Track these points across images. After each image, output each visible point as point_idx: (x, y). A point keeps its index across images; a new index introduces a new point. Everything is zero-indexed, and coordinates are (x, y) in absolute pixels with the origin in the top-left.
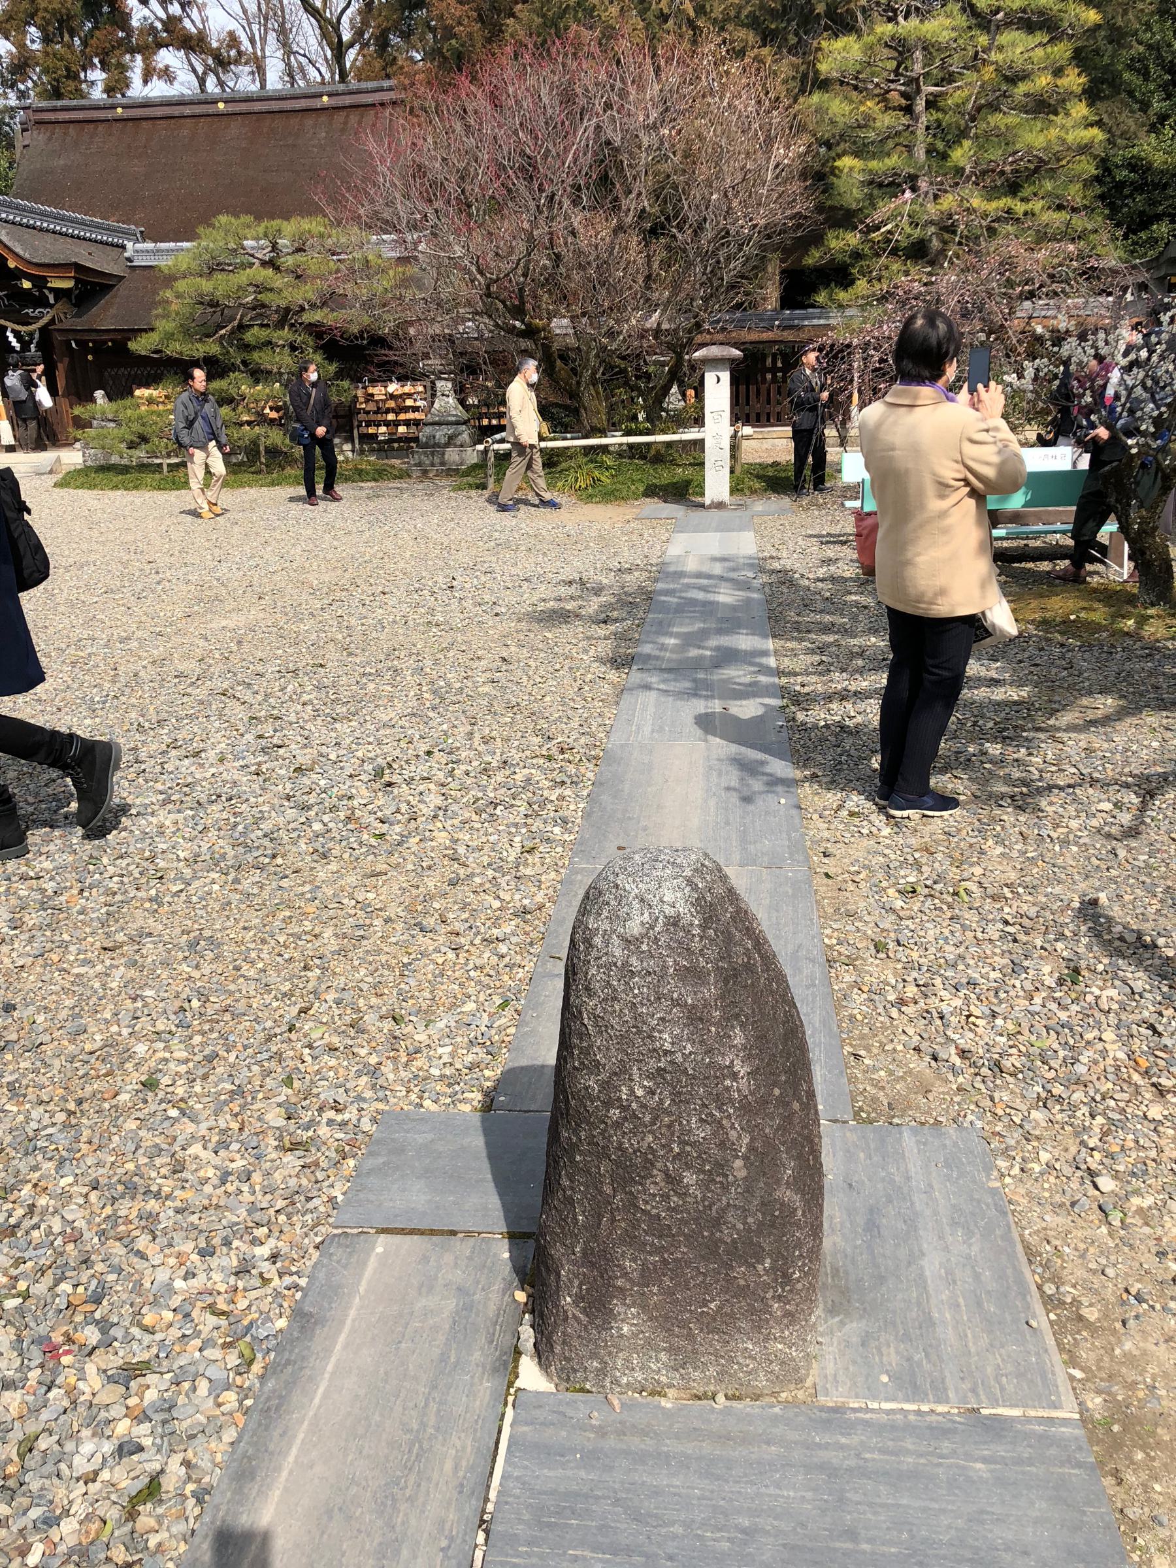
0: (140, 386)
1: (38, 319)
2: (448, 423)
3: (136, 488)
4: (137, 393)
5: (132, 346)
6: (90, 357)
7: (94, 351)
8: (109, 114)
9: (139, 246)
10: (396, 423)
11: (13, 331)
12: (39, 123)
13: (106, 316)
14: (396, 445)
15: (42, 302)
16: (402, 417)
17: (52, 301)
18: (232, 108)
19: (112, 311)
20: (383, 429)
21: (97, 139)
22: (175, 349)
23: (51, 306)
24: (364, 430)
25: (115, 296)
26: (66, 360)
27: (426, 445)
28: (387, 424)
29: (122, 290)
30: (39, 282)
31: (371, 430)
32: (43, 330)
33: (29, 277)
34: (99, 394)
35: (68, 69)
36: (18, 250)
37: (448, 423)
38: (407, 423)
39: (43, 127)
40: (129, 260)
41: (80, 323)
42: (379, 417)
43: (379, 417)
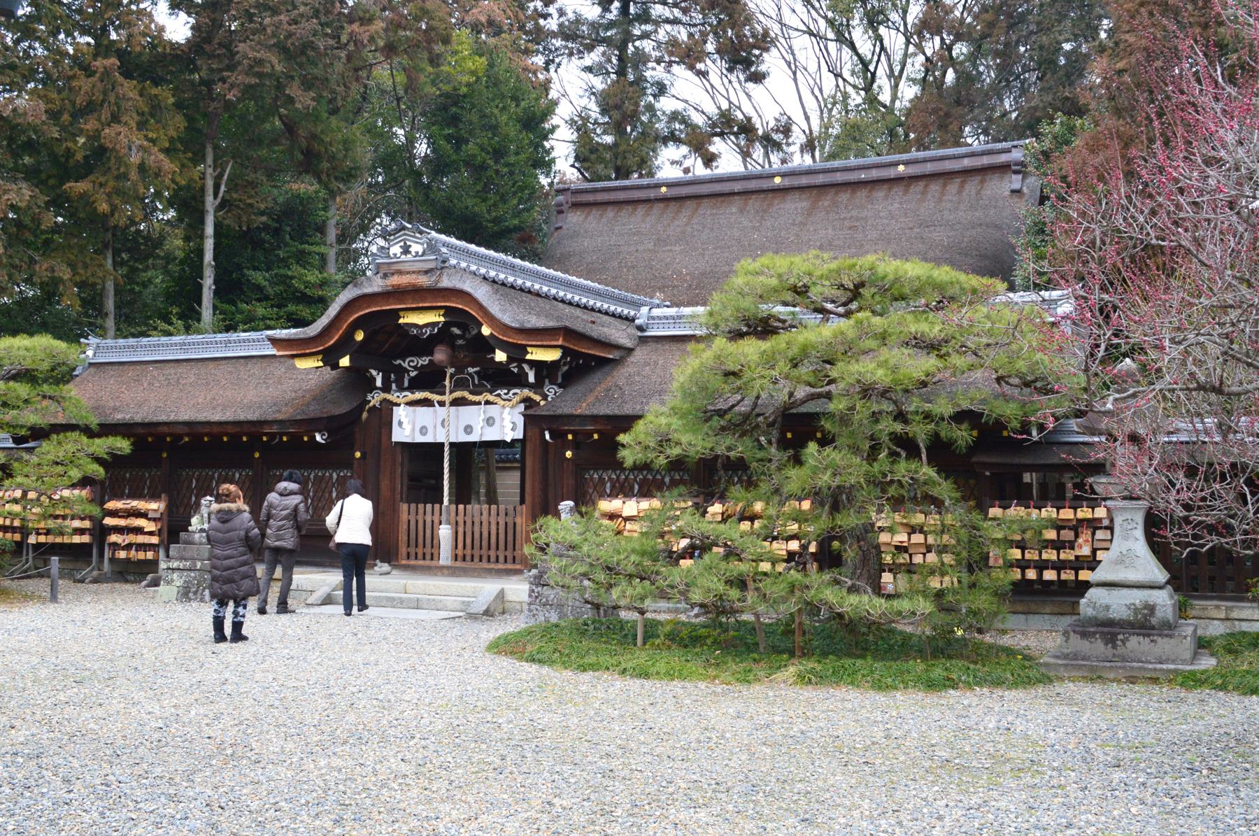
6: (569, 454)
7: (575, 446)
16: (1031, 555)
18: (788, 182)
30: (517, 353)
33: (505, 346)
40: (640, 328)
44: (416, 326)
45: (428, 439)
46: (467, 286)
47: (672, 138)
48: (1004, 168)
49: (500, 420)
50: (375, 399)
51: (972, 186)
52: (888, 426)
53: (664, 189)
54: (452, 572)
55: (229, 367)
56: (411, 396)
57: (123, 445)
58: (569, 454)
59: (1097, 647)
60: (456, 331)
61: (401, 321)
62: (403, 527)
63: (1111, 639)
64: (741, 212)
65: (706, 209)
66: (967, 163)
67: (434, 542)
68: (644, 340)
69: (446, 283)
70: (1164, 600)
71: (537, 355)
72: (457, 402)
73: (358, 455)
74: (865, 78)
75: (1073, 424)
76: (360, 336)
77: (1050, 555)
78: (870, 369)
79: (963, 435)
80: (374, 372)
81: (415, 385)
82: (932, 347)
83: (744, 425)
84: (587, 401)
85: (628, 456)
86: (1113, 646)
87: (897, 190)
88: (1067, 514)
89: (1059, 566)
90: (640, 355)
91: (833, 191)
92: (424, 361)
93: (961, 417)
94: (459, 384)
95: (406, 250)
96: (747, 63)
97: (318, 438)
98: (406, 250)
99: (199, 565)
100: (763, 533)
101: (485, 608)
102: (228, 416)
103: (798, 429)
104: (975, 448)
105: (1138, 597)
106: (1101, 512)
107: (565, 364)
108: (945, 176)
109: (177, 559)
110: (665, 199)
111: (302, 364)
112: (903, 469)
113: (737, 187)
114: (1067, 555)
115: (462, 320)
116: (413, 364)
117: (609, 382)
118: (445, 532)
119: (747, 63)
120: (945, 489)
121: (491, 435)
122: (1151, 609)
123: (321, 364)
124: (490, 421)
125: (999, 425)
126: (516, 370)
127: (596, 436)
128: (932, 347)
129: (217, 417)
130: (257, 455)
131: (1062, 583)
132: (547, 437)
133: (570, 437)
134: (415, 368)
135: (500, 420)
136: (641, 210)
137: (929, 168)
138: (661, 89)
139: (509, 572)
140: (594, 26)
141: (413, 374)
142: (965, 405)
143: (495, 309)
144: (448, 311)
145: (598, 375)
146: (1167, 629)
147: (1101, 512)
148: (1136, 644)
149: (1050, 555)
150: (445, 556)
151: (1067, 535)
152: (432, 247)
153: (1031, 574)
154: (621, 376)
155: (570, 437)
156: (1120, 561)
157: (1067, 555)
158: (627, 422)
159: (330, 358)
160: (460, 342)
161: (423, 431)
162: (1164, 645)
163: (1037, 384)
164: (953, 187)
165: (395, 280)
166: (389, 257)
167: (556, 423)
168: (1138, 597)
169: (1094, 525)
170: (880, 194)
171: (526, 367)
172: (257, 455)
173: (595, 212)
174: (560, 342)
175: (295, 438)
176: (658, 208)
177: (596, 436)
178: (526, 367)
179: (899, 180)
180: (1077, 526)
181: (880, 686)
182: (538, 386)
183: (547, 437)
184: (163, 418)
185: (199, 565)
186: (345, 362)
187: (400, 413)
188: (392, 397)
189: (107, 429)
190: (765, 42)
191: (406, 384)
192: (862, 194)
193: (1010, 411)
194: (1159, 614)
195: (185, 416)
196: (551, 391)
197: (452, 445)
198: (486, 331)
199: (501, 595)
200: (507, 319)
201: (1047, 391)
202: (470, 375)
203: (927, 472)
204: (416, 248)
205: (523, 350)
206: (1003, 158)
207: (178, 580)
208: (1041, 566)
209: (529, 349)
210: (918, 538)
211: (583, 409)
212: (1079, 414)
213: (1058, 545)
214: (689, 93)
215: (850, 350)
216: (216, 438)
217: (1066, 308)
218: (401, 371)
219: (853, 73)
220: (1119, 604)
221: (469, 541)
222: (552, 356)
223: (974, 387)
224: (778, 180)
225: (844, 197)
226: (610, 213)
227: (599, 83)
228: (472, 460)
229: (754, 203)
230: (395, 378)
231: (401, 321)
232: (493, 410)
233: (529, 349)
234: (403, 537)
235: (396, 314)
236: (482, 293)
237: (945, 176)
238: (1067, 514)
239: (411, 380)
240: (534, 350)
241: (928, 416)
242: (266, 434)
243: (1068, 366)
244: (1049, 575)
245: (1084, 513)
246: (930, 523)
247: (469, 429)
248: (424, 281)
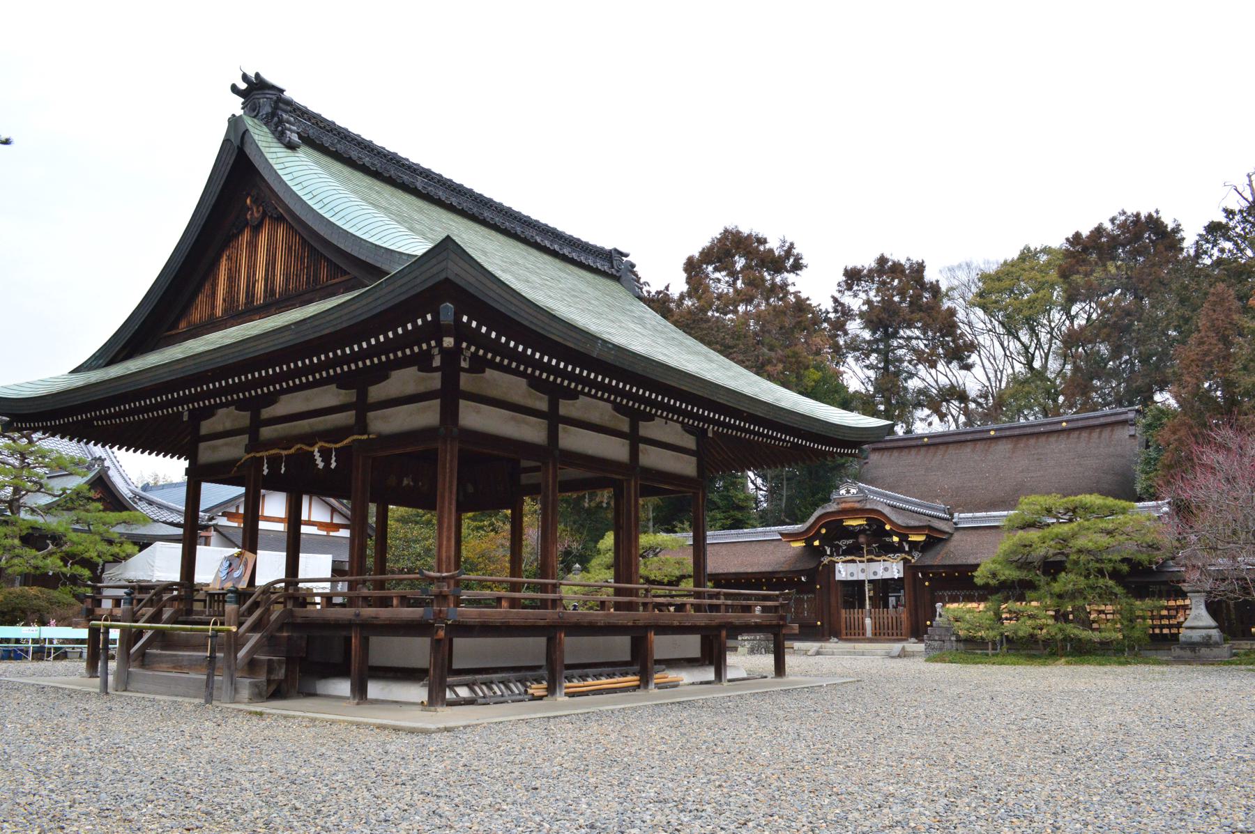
7: (930, 580)
9: (962, 515)
18: (999, 434)
30: (904, 537)
33: (897, 534)
45: (855, 578)
46: (879, 508)
47: (919, 405)
48: (1124, 423)
49: (892, 569)
50: (826, 560)
51: (1106, 433)
52: (1093, 565)
54: (870, 641)
55: (757, 547)
56: (844, 559)
59: (1188, 653)
62: (843, 620)
63: (1193, 650)
64: (973, 451)
65: (952, 450)
66: (1102, 420)
67: (864, 628)
68: (957, 529)
69: (868, 506)
70: (1215, 633)
71: (913, 538)
72: (870, 561)
74: (1027, 357)
75: (1171, 563)
76: (824, 531)
77: (1165, 622)
78: (1081, 542)
79: (1125, 568)
81: (845, 553)
82: (1110, 533)
83: (1025, 565)
84: (938, 558)
85: (979, 581)
86: (1195, 653)
87: (1063, 437)
88: (1172, 603)
89: (1170, 627)
90: (957, 536)
91: (1025, 439)
93: (1124, 560)
94: (869, 552)
95: (848, 492)
96: (961, 359)
98: (848, 492)
100: (1035, 613)
102: (755, 569)
103: (1052, 568)
104: (1129, 574)
105: (1204, 632)
106: (1187, 602)
108: (1091, 428)
110: (927, 445)
112: (1101, 582)
113: (969, 437)
114: (1173, 622)
116: (844, 543)
117: (945, 550)
118: (868, 621)
119: (961, 359)
120: (1118, 590)
121: (887, 576)
122: (1210, 637)
124: (886, 569)
125: (1140, 563)
128: (1110, 533)
129: (750, 570)
131: (1172, 635)
135: (892, 569)
136: (914, 452)
137: (1080, 424)
138: (911, 375)
140: (869, 342)
142: (1125, 556)
143: (893, 517)
144: (868, 519)
145: (939, 547)
146: (1216, 645)
147: (1187, 602)
148: (1204, 651)
149: (1165, 622)
150: (869, 633)
151: (1173, 613)
152: (861, 490)
153: (1157, 631)
154: (952, 545)
156: (1196, 618)
157: (1173, 622)
158: (976, 566)
161: (852, 574)
162: (1216, 651)
163: (1153, 547)
164: (1095, 434)
165: (843, 505)
167: (925, 569)
168: (1204, 632)
169: (1185, 608)
170: (1053, 439)
173: (887, 454)
176: (923, 450)
179: (1063, 430)
180: (1178, 608)
181: (1100, 664)
182: (909, 553)
184: (721, 571)
187: (840, 566)
188: (835, 559)
190: (972, 347)
192: (1043, 439)
193: (1143, 557)
194: (1213, 639)
195: (733, 570)
196: (917, 555)
197: (870, 581)
198: (888, 527)
199: (903, 648)
200: (899, 522)
201: (1159, 549)
203: (1111, 583)
204: (853, 491)
206: (1123, 417)
207: (748, 645)
208: (1162, 627)
210: (1103, 616)
211: (937, 562)
212: (1173, 558)
213: (1169, 617)
214: (923, 379)
215: (1074, 535)
217: (1166, 509)
219: (1019, 353)
220: (1196, 635)
222: (921, 538)
223: (1130, 550)
224: (992, 433)
225: (1032, 441)
226: (896, 453)
227: (872, 374)
228: (884, 588)
229: (980, 446)
230: (837, 551)
232: (887, 564)
234: (843, 625)
235: (842, 521)
236: (886, 511)
237: (1091, 428)
238: (1172, 603)
241: (1110, 560)
243: (1167, 539)
244: (1166, 631)
245: (1180, 602)
246: (1114, 607)
247: (875, 573)
248: (857, 505)
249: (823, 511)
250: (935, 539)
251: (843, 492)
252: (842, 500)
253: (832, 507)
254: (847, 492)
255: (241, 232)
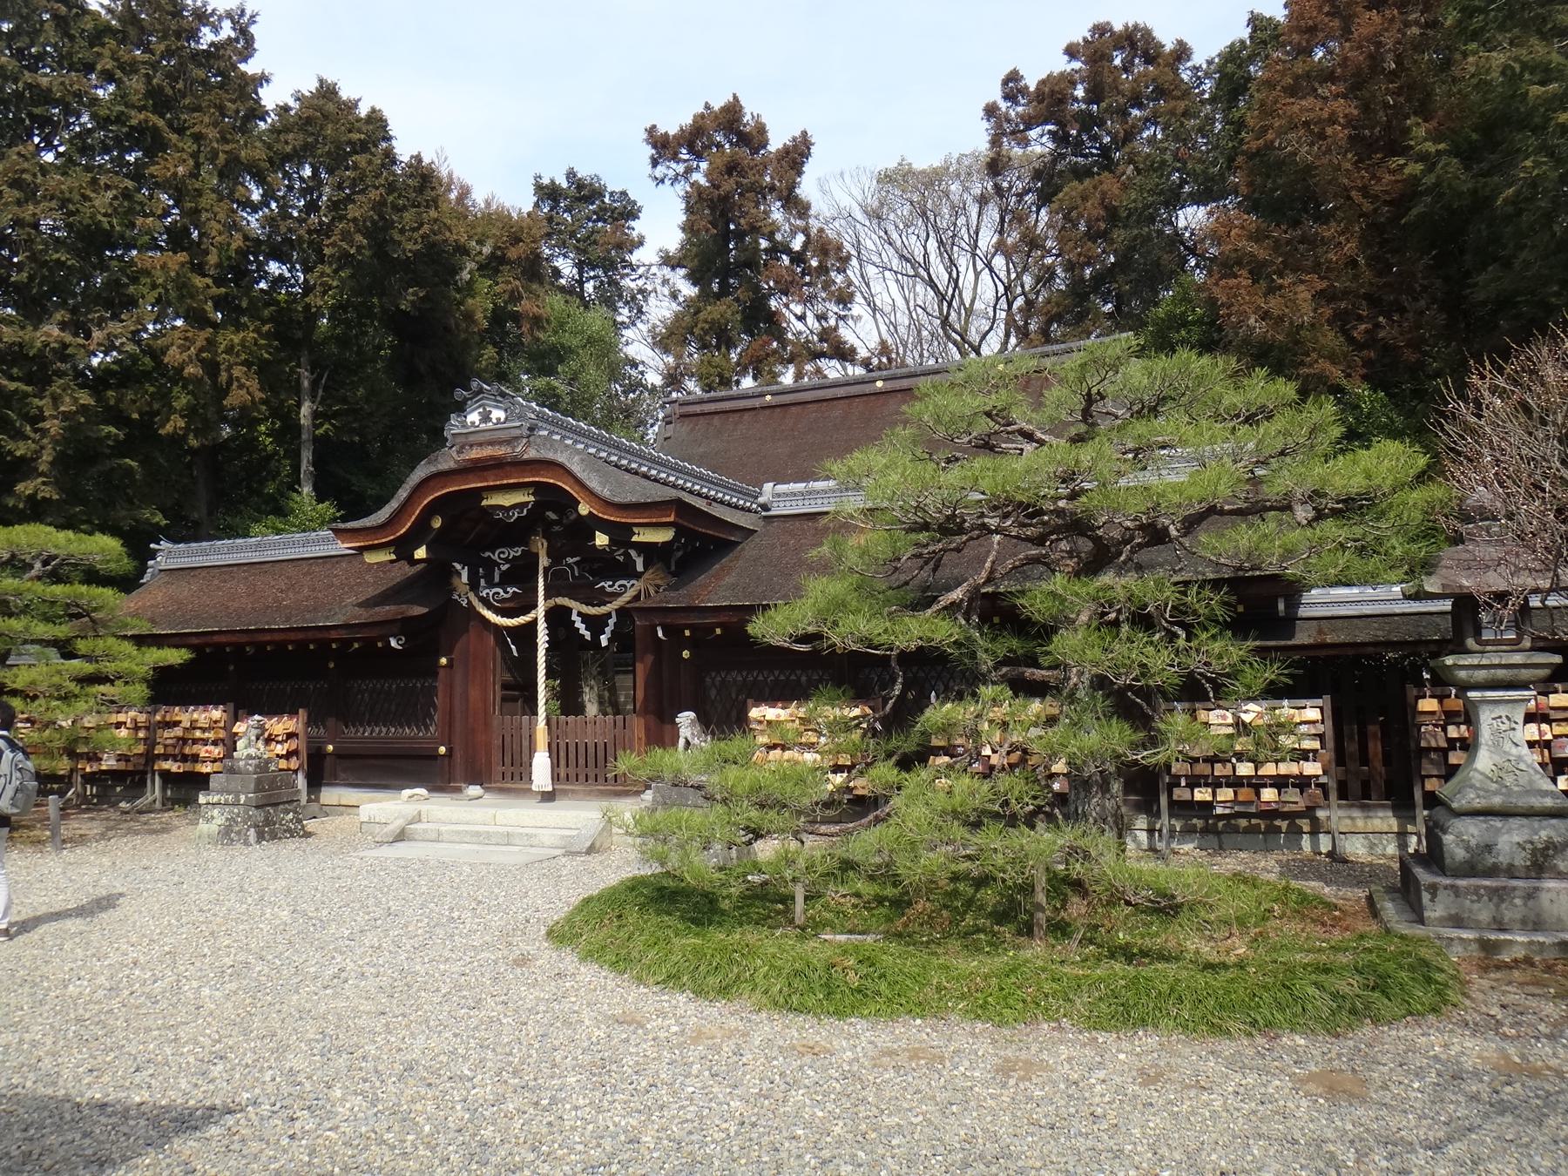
0: (757, 703)
1: (616, 595)
2: (1530, 813)
3: (724, 991)
4: (754, 713)
5: (758, 627)
6: (686, 654)
7: (692, 644)
8: (757, 403)
9: (782, 488)
10: (1256, 784)
11: (579, 614)
12: (683, 416)
13: (717, 589)
14: (1243, 823)
15: (628, 572)
16: (1269, 769)
17: (640, 568)
18: (891, 385)
19: (728, 580)
20: (1226, 794)
21: (740, 426)
22: (858, 628)
23: (638, 576)
24: (1181, 794)
25: (737, 558)
26: (650, 658)
27: (1471, 869)
28: (1236, 782)
29: (749, 549)
30: (620, 534)
31: (1202, 794)
32: (621, 612)
33: (606, 527)
34: (686, 719)
35: (720, 375)
36: (594, 484)
37: (1530, 813)
38: (1280, 782)
39: (687, 420)
40: (765, 507)
41: (675, 599)
42: (1219, 770)
43: (1219, 770)
44: (501, 507)
53: (768, 398)
54: (548, 797)
57: (175, 656)
58: (686, 654)
60: (552, 515)
61: (484, 503)
73: (444, 661)
76: (437, 523)
80: (458, 566)
92: (517, 552)
95: (486, 418)
97: (393, 643)
98: (486, 418)
99: (243, 798)
101: (588, 844)
107: (678, 549)
109: (218, 792)
111: (372, 558)
115: (553, 501)
123: (393, 557)
126: (621, 559)
127: (718, 631)
130: (332, 665)
132: (660, 634)
133: (687, 633)
134: (507, 560)
139: (618, 794)
141: (504, 568)
155: (687, 633)
159: (403, 549)
160: (557, 528)
165: (475, 454)
166: (464, 426)
171: (633, 553)
172: (332, 665)
174: (672, 519)
175: (369, 643)
177: (718, 631)
178: (633, 553)
183: (660, 634)
185: (243, 798)
186: (421, 553)
189: (158, 641)
191: (497, 579)
202: (569, 565)
205: (628, 529)
209: (636, 530)
216: (281, 645)
218: (491, 565)
221: (572, 756)
224: (879, 384)
231: (484, 503)
233: (636, 530)
239: (503, 574)
240: (641, 530)
242: (334, 640)
249: (433, 469)
250: (701, 540)
251: (474, 417)
252: (470, 439)
253: (447, 460)
254: (483, 419)
255: (859, 696)
